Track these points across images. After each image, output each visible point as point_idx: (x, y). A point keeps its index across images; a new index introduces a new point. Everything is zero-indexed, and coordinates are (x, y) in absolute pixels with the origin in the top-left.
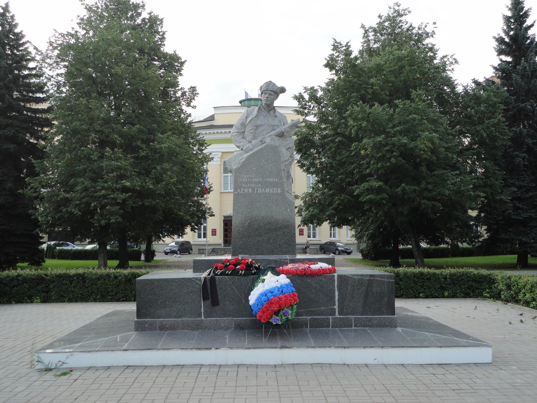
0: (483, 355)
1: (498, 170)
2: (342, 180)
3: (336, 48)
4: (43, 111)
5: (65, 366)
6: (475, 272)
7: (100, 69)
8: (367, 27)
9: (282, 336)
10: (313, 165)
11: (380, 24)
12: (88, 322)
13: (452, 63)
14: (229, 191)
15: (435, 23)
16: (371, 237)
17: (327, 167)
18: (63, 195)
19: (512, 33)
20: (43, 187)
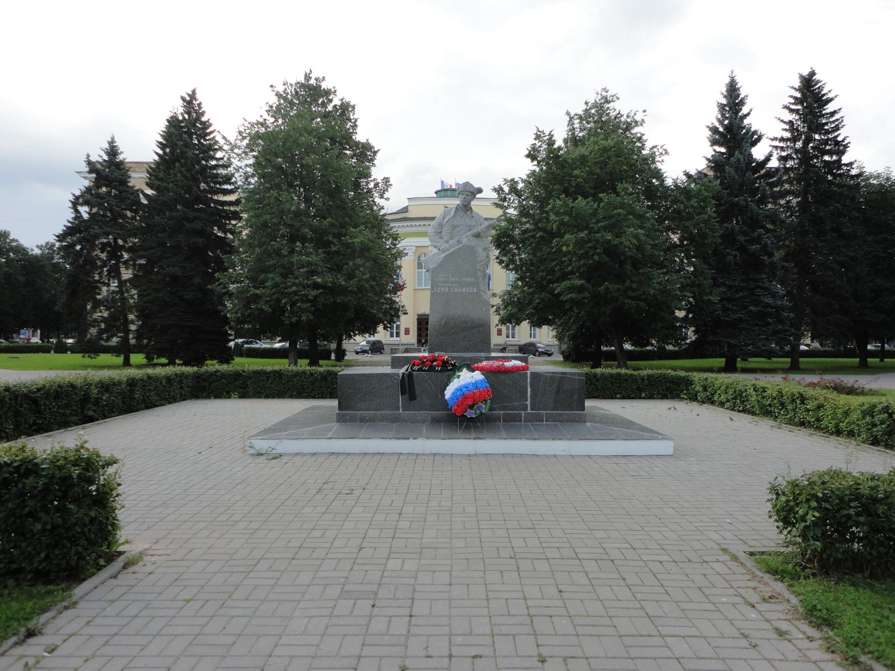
0: (665, 447)
1: (708, 269)
2: (542, 278)
3: (538, 137)
4: (231, 203)
5: (274, 452)
6: (673, 373)
7: (292, 161)
8: (572, 114)
9: (476, 428)
10: (512, 261)
11: (586, 111)
12: (288, 416)
13: (661, 154)
14: (423, 287)
15: (645, 111)
16: (573, 338)
17: (526, 264)
18: (253, 291)
19: (726, 122)
20: (233, 283)
